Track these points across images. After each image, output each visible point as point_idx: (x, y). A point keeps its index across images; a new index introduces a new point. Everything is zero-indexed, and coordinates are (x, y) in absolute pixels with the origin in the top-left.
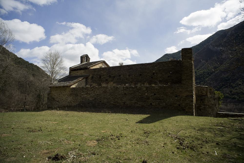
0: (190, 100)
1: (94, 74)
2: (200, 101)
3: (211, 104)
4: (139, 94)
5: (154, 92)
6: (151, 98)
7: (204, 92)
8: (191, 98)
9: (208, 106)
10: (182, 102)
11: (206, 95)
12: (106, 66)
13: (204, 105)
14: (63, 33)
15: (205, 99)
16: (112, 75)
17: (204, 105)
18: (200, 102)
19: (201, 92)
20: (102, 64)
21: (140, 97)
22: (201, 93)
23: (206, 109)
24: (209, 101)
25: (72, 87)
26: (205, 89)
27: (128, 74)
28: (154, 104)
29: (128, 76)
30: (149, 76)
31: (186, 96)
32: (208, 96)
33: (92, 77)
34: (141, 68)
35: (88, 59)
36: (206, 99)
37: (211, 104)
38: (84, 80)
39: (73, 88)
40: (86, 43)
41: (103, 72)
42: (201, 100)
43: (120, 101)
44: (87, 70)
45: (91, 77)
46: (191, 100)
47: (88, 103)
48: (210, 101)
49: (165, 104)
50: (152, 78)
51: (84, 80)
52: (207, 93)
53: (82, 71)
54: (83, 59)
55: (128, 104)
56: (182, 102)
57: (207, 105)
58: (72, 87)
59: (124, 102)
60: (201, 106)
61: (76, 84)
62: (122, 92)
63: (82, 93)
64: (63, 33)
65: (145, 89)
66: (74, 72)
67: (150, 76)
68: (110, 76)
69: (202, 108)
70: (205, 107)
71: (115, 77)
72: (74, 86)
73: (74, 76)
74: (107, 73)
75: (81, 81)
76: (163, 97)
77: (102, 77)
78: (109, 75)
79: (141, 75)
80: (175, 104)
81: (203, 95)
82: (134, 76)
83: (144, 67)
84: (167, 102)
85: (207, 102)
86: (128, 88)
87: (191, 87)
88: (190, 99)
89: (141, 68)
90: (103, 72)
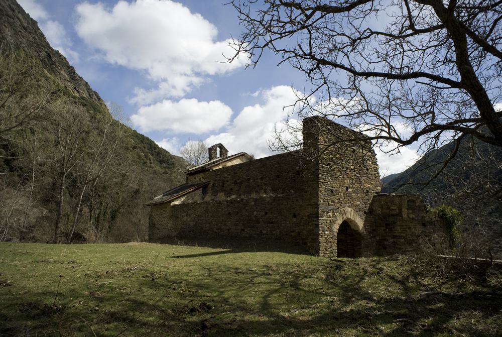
0: (314, 223)
1: (216, 180)
2: (385, 228)
3: (411, 235)
4: (247, 213)
5: (264, 210)
6: (261, 220)
7: (396, 208)
8: (315, 219)
9: (403, 240)
10: (302, 227)
11: (400, 214)
12: (245, 161)
13: (394, 237)
14: (224, 103)
15: (394, 223)
16: (238, 179)
17: (394, 237)
18: (384, 230)
19: (389, 208)
20: (240, 160)
21: (247, 218)
22: (388, 211)
23: (399, 247)
24: (405, 227)
25: (173, 203)
26: (397, 200)
27: (260, 177)
28: (265, 232)
29: (259, 181)
30: (291, 177)
31: (308, 215)
32: (402, 217)
33: (214, 185)
34: (278, 163)
35: (224, 151)
36: (398, 223)
37: (411, 235)
38: (199, 192)
39: (175, 206)
40: (496, 111)
41: (226, 175)
42: (387, 225)
43: (224, 227)
44: (207, 173)
45: (211, 185)
46: (316, 223)
47: (190, 232)
48: (410, 228)
49: (278, 231)
50: (295, 180)
51: (199, 192)
52: (401, 209)
53: (201, 175)
54: (212, 153)
55: (233, 233)
56: (302, 227)
57: (400, 237)
58: (173, 203)
59: (228, 228)
60: (387, 238)
61: (182, 199)
62: (226, 210)
63: (183, 214)
64: (224, 103)
65: (253, 203)
66: (192, 177)
67: (291, 178)
68: (236, 181)
69: (387, 243)
70: (395, 240)
71: (242, 183)
72: (177, 202)
73: (191, 184)
74: (232, 176)
75: (193, 193)
76: (276, 217)
77: (226, 185)
78: (235, 180)
79: (278, 176)
80: (293, 232)
81: (390, 214)
82: (269, 178)
83: (283, 160)
84: (281, 227)
85: (400, 231)
86: (232, 203)
87: (315, 196)
88: (313, 221)
89: (278, 163)
90: (226, 175)
